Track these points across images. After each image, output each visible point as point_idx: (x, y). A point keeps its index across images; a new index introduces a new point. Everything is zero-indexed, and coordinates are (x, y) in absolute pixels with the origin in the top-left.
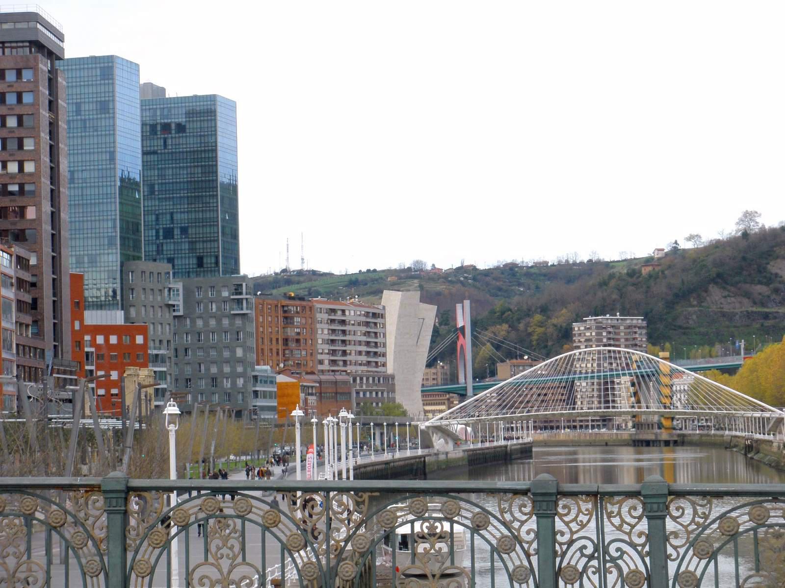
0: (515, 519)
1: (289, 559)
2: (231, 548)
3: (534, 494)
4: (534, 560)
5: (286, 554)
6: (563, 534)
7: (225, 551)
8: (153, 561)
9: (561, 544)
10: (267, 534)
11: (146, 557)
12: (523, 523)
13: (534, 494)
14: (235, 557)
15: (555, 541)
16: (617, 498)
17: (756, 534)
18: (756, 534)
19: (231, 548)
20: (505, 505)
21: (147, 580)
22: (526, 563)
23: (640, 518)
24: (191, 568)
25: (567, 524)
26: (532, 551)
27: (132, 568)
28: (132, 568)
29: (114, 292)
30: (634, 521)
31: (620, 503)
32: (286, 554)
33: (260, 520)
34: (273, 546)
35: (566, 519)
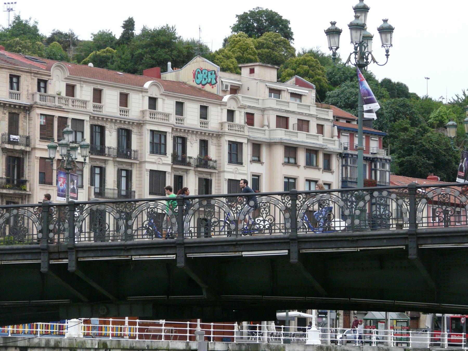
0: (286, 201)
1: (34, 224)
2: (266, 211)
3: (409, 188)
4: (409, 207)
5: (281, 212)
6: (239, 207)
7: (264, 212)
8: (190, 218)
9: (298, 207)
10: (335, 204)
11: (421, 207)
12: (288, 202)
13: (409, 188)
14: (267, 214)
15: (296, 206)
16: (118, 203)
17: (438, 196)
18: (438, 196)
19: (266, 211)
20: (118, 206)
21: (421, 213)
22: (406, 208)
23: (289, 201)
24: (143, 222)
25: (300, 202)
26: (408, 205)
27: (298, 215)
28: (298, 215)
29: (327, 149)
30: (288, 201)
31: (119, 204)
32: (281, 212)
33: (161, 208)
34: (31, 222)
35: (300, 200)
